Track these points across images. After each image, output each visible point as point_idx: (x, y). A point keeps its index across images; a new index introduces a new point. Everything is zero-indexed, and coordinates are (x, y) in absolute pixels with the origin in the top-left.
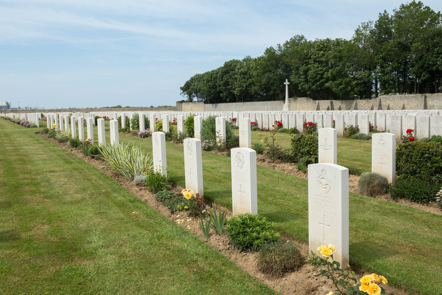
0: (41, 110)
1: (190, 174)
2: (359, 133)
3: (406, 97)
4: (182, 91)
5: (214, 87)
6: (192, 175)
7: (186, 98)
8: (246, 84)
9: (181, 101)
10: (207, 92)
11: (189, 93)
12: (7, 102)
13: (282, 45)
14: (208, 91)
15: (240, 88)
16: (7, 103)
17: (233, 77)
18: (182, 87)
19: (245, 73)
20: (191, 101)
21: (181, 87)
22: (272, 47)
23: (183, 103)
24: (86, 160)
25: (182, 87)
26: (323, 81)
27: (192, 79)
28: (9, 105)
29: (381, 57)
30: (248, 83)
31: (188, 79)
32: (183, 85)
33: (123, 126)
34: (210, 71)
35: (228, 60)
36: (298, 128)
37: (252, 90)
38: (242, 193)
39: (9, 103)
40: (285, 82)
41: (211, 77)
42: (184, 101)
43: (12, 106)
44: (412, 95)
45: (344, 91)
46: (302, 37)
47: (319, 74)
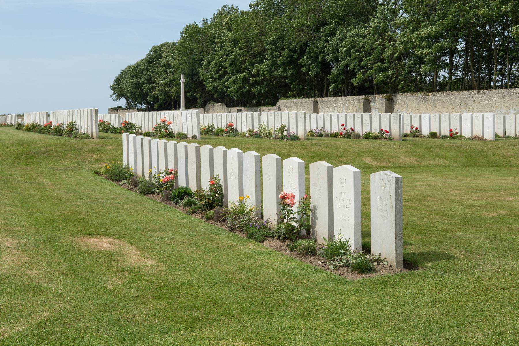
13: (209, 19)
14: (131, 92)
22: (195, 23)
31: (118, 73)
32: (112, 83)
40: (181, 79)
45: (240, 93)
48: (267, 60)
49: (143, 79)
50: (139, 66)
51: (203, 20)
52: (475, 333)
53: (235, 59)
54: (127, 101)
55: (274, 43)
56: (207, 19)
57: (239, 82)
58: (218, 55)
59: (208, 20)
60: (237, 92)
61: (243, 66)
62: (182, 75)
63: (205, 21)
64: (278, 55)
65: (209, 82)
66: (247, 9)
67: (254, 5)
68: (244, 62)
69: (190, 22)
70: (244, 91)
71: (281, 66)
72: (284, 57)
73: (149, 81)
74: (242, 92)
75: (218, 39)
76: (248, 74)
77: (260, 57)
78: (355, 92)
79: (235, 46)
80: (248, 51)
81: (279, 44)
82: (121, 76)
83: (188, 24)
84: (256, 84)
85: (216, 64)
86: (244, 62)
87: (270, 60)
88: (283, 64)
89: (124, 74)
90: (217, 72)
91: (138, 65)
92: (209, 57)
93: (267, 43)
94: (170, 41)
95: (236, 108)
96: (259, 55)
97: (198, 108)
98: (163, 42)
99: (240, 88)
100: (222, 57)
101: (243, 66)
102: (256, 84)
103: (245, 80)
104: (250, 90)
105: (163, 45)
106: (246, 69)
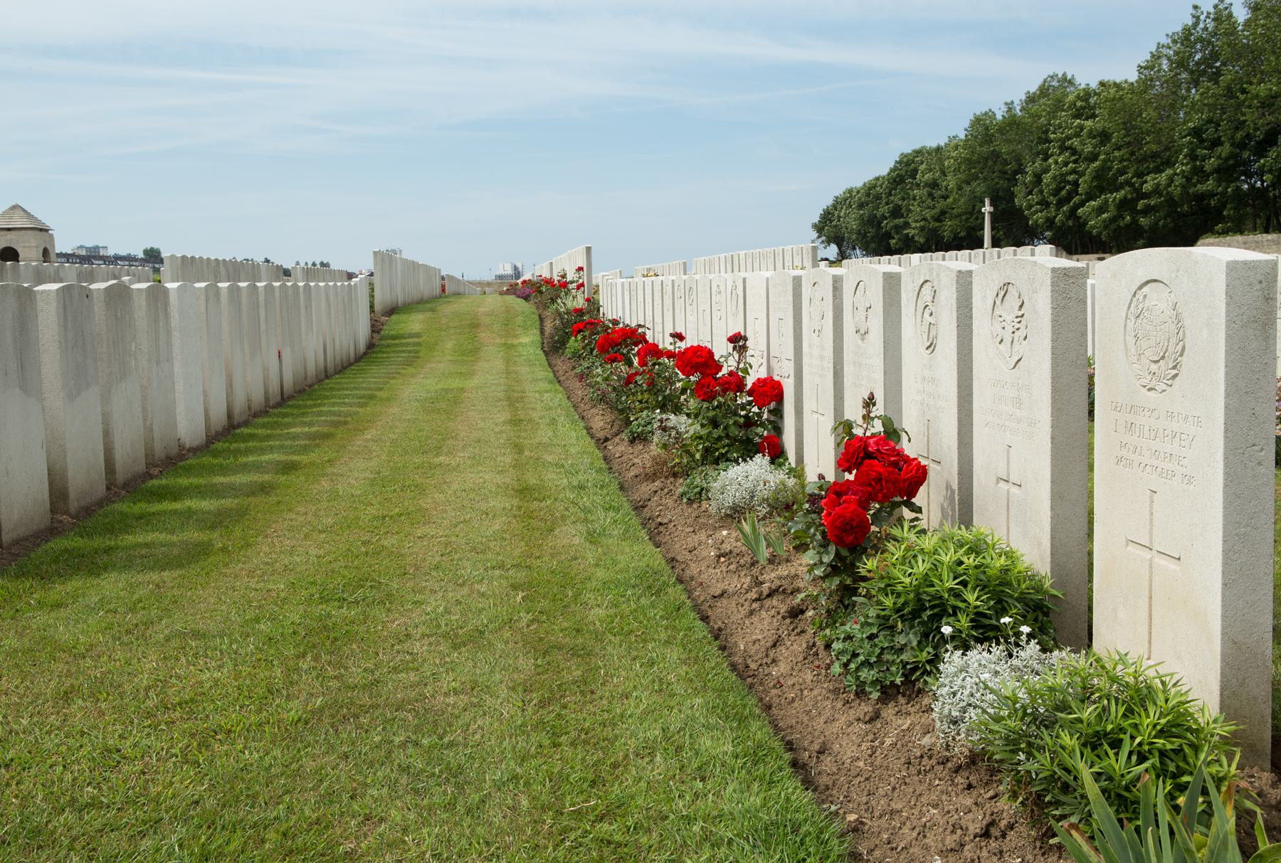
0: (483, 283)
1: (1002, 485)
3: (1257, 242)
6: (1014, 490)
8: (933, 212)
11: (862, 235)
12: (515, 267)
13: (1017, 102)
14: (859, 233)
15: (922, 223)
16: (516, 268)
22: (990, 110)
26: (1077, 202)
28: (519, 273)
29: (1190, 129)
30: (937, 211)
31: (829, 202)
32: (816, 219)
34: (858, 183)
35: (908, 150)
38: (1162, 562)
39: (520, 269)
40: (984, 206)
44: (1270, 237)
45: (1113, 226)
46: (1067, 81)
47: (1069, 182)
48: (1182, 164)
49: (884, 210)
50: (875, 187)
51: (1006, 104)
52: (248, 636)
53: (1104, 168)
54: (840, 248)
55: (1196, 132)
56: (1012, 103)
57: (1112, 208)
58: (1056, 162)
59: (1015, 104)
60: (1106, 227)
61: (1122, 179)
62: (986, 200)
63: (1010, 106)
64: (1205, 155)
65: (1036, 212)
66: (1133, 77)
67: (1146, 68)
68: (1122, 172)
69: (980, 110)
70: (1122, 224)
71: (1212, 175)
72: (1219, 157)
73: (896, 212)
74: (1118, 226)
75: (1054, 133)
76: (1131, 194)
77: (1154, 162)
78: (1079, 251)
79: (1103, 143)
80: (1133, 153)
81: (1210, 133)
82: (835, 207)
83: (978, 113)
84: (1147, 211)
85: (1054, 178)
86: (1122, 172)
87: (1187, 164)
88: (1217, 170)
89: (838, 203)
90: (1056, 192)
91: (870, 188)
92: (1036, 167)
93: (1180, 134)
94: (932, 144)
95: (1097, 256)
96: (1152, 157)
97: (1225, 232)
98: (917, 146)
99: (1113, 220)
100: (1066, 164)
101: (1122, 179)
102: (1147, 211)
103: (1124, 205)
104: (1135, 222)
105: (918, 152)
106: (1128, 183)
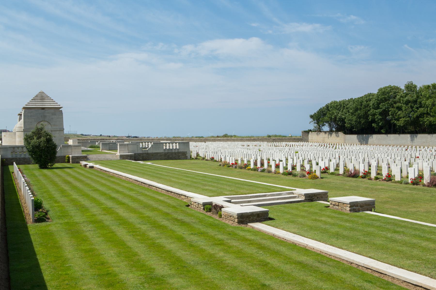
2: (373, 178)
4: (312, 120)
5: (366, 116)
7: (312, 126)
9: (307, 130)
10: (355, 121)
17: (395, 105)
18: (312, 115)
19: (415, 102)
20: (319, 130)
21: (312, 115)
23: (310, 133)
24: (204, 212)
25: (312, 115)
27: (327, 106)
32: (312, 114)
33: (344, 166)
36: (217, 160)
37: (426, 120)
41: (361, 105)
42: (311, 131)
43: (324, 133)
